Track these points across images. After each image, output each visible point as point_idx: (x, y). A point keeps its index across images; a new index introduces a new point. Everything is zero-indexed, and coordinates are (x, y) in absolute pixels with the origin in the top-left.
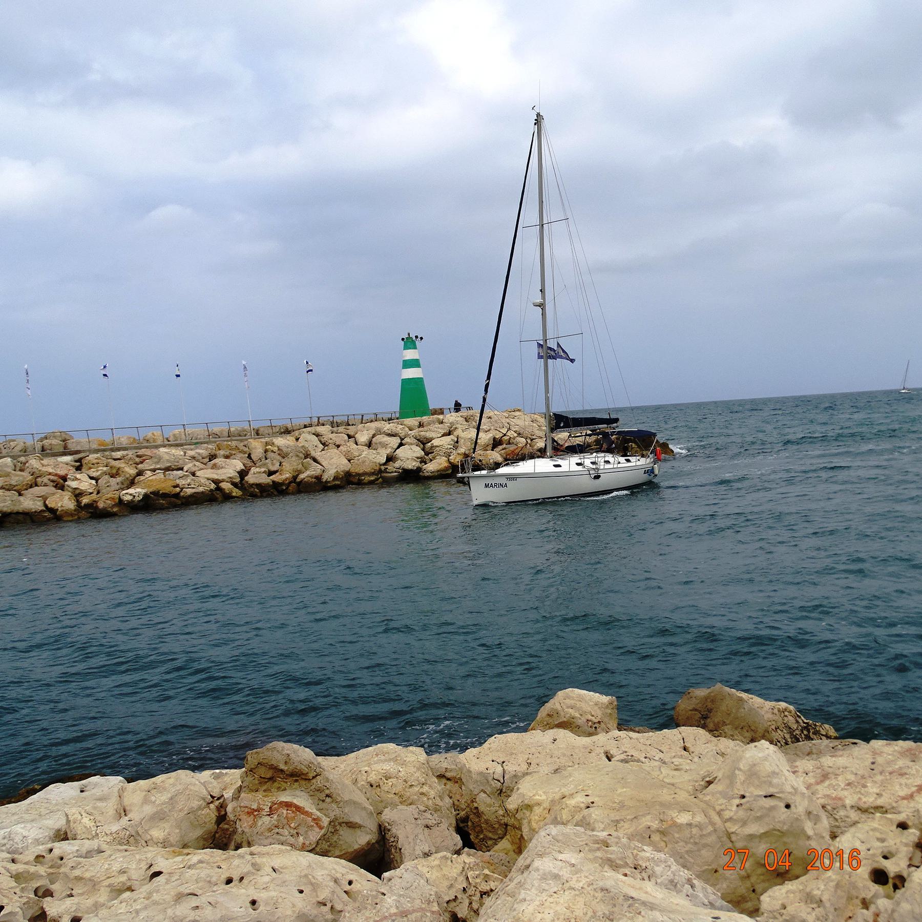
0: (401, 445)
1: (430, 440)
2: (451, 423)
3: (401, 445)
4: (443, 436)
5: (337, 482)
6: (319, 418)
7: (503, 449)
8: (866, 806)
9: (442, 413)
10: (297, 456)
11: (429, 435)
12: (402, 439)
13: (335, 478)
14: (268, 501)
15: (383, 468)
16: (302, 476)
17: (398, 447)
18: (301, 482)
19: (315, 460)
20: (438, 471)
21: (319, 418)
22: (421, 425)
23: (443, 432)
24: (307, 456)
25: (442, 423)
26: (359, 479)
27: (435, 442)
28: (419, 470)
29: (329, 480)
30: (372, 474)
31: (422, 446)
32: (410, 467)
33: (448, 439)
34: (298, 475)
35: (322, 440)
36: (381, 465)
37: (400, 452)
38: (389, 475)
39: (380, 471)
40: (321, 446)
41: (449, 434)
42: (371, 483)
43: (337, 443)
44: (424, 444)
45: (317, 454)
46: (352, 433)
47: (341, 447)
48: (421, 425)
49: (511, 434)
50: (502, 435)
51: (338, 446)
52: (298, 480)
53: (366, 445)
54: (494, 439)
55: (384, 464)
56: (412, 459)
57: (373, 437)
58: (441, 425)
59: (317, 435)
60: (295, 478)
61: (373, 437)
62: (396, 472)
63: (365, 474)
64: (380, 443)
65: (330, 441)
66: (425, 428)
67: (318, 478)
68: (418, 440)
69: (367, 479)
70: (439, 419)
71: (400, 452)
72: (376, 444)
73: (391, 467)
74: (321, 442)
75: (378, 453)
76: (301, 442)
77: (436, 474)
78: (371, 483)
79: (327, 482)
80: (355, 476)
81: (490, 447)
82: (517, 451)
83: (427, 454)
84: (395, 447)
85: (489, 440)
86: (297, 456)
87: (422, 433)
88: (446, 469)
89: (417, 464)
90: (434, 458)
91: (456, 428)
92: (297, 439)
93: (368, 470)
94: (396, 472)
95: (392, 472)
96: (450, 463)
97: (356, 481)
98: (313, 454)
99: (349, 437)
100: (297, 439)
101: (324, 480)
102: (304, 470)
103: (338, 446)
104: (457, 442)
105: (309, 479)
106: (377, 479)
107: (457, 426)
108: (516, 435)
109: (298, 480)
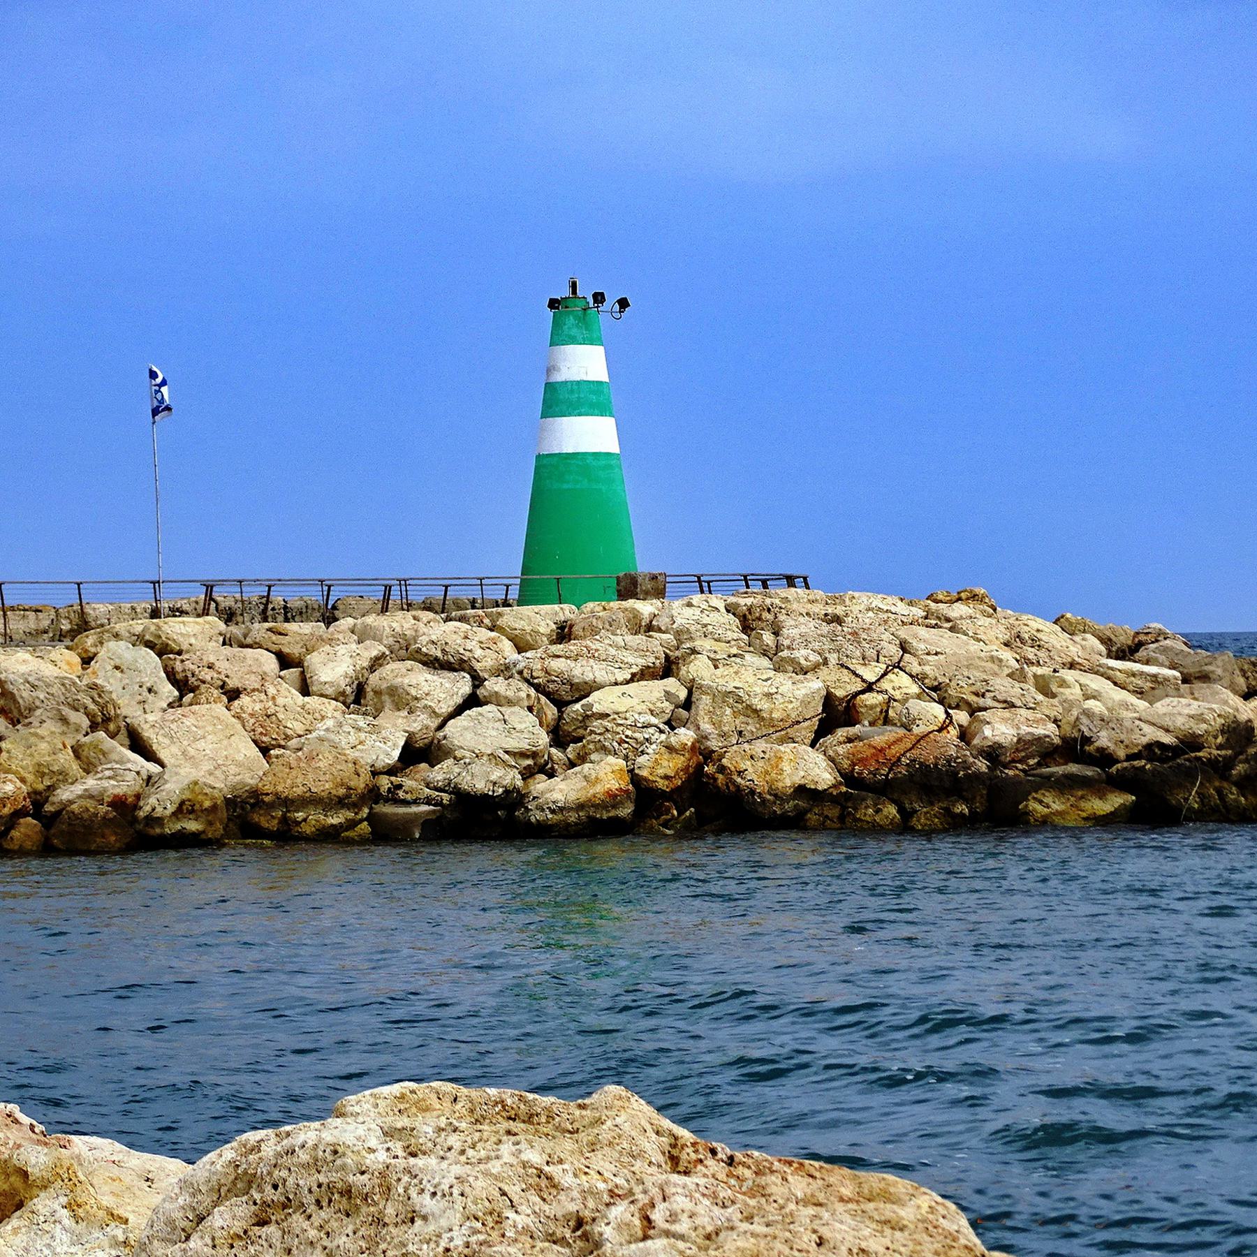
0: (472, 701)
1: (584, 690)
2: (678, 633)
3: (472, 701)
4: (633, 679)
5: (193, 826)
6: (209, 588)
7: (850, 740)
8: (1220, 1101)
9: (660, 593)
10: (64, 720)
11: (582, 671)
12: (477, 681)
13: (186, 810)
14: (393, 852)
15: (385, 782)
16: (65, 794)
17: (458, 711)
18: (58, 813)
19: (139, 745)
20: (581, 806)
21: (209, 588)
22: (564, 633)
23: (638, 662)
24: (102, 720)
25: (650, 628)
26: (284, 820)
27: (600, 701)
28: (514, 799)
29: (159, 812)
30: (340, 803)
31: (551, 711)
32: (481, 786)
33: (654, 690)
34: (51, 788)
35: (178, 667)
36: (375, 773)
37: (460, 732)
38: (402, 810)
39: (373, 795)
40: (169, 691)
41: (668, 669)
42: (329, 836)
43: (232, 683)
44: (560, 704)
45: (150, 725)
46: (293, 650)
47: (245, 700)
48: (564, 633)
49: (900, 683)
50: (859, 686)
51: (233, 694)
52: (48, 808)
53: (340, 697)
54: (829, 699)
55: (391, 771)
56: (492, 756)
57: (372, 669)
58: (640, 639)
59: (162, 650)
60: (38, 800)
61: (372, 669)
62: (428, 801)
63: (310, 801)
64: (393, 691)
65: (207, 675)
66: (572, 647)
67: (124, 807)
68: (537, 688)
69: (312, 819)
70: (636, 615)
71: (460, 732)
72: (378, 693)
73: (411, 783)
74: (171, 676)
75: (375, 729)
76: (102, 673)
77: (572, 817)
78: (329, 836)
79: (152, 820)
80: (271, 806)
81: (807, 730)
82: (895, 750)
83: (559, 737)
84: (445, 708)
85: (805, 703)
86: (64, 720)
87: (557, 665)
88: (613, 799)
89: (512, 778)
90: (582, 758)
91: (694, 651)
92: (87, 661)
93: (324, 786)
94: (428, 801)
95: (416, 802)
96: (635, 779)
97: (273, 825)
98: (129, 710)
99: (285, 661)
100: (87, 661)
101: (142, 814)
102: (75, 767)
103: (233, 694)
104: (688, 704)
105: (90, 804)
106: (352, 824)
107: (699, 644)
108: (914, 689)
109: (48, 808)
